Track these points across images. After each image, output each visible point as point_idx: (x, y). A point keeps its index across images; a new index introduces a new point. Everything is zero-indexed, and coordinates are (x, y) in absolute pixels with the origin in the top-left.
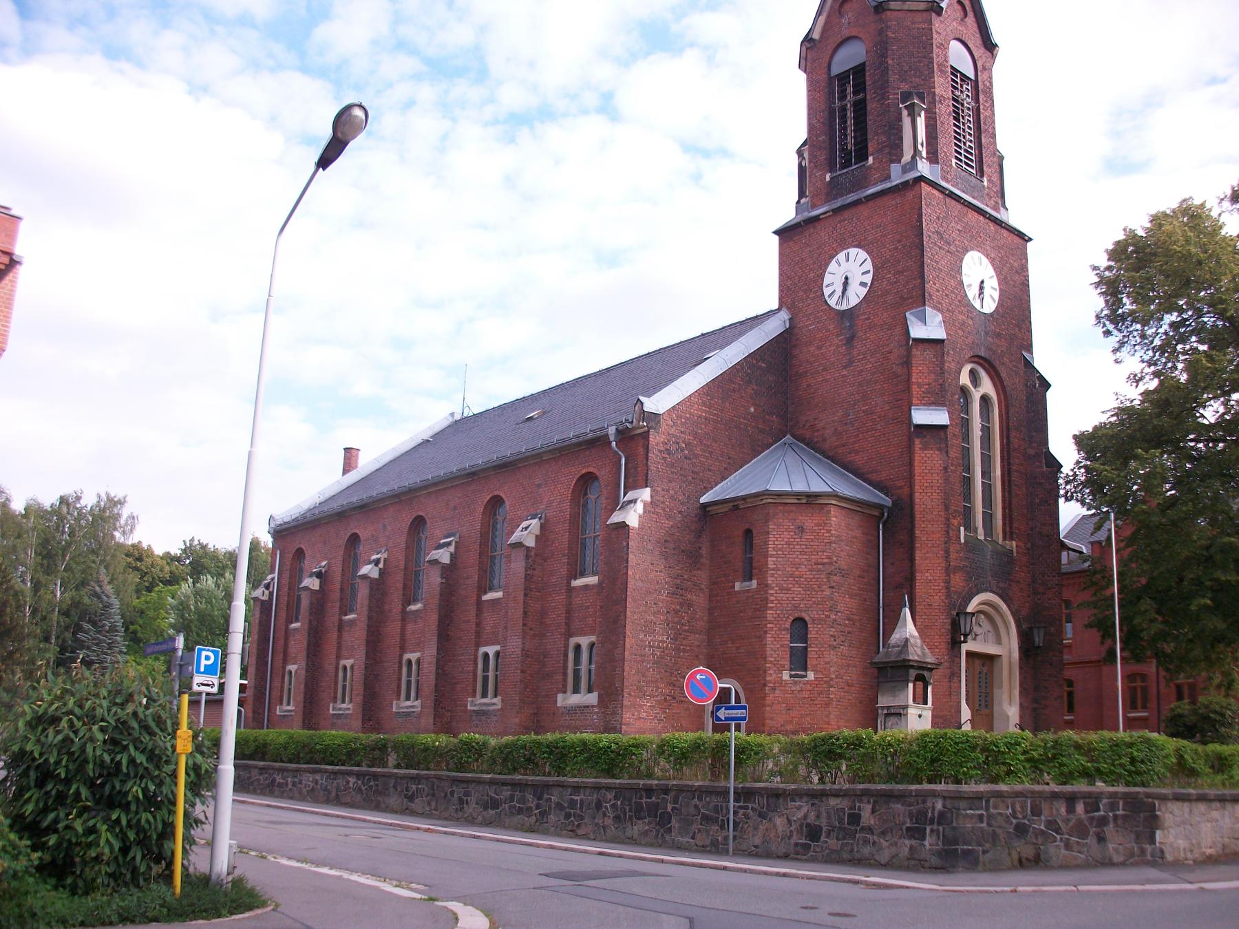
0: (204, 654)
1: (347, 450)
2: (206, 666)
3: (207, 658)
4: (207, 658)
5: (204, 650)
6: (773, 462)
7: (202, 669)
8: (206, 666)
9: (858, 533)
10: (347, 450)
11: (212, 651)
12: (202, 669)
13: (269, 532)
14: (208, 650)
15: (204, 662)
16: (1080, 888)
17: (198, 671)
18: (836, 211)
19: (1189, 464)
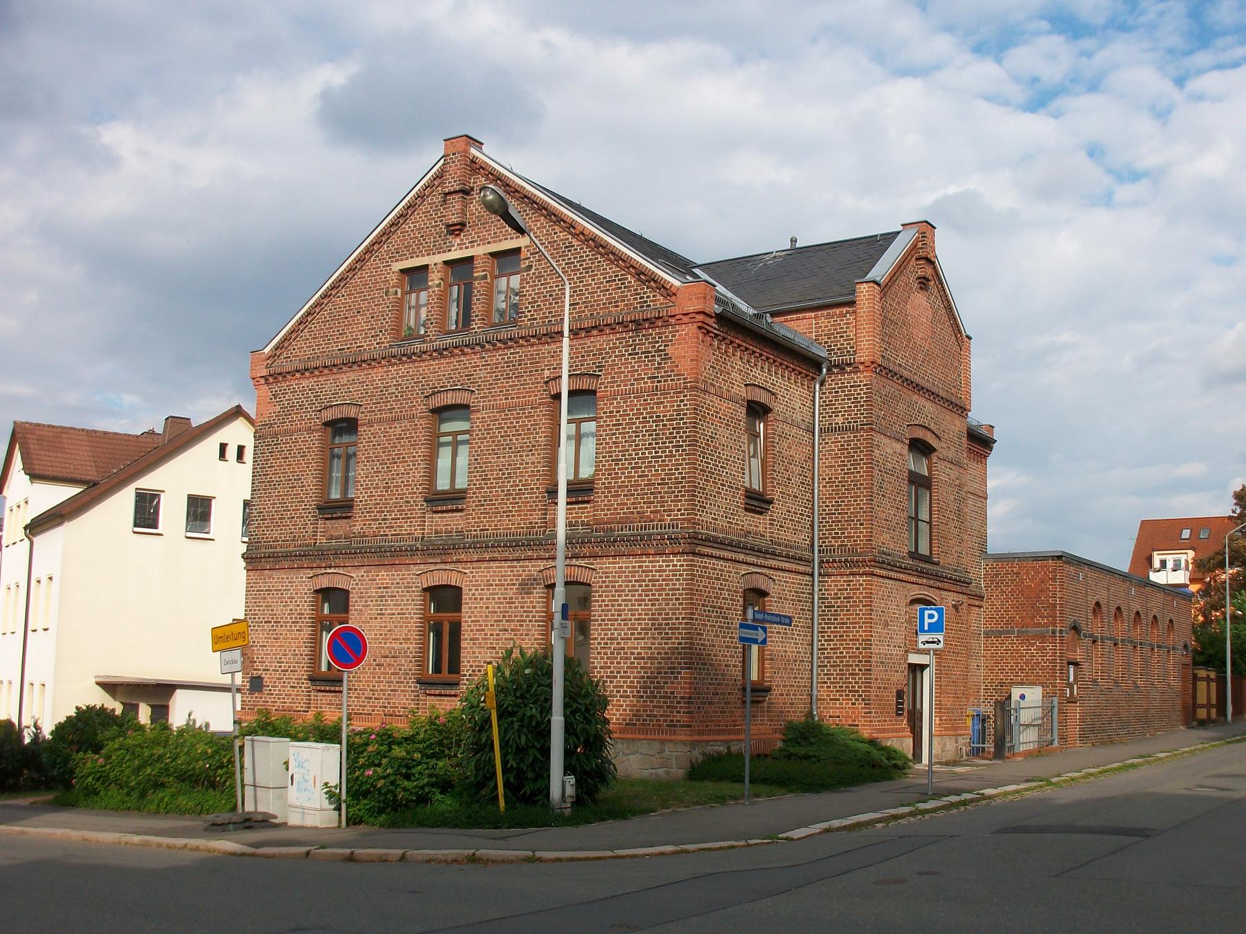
0: (927, 613)
1: (239, 446)
2: (929, 624)
3: (931, 616)
4: (931, 616)
5: (927, 609)
6: (1214, 739)
7: (926, 628)
8: (929, 624)
9: (7, 794)
10: (239, 446)
11: (935, 610)
12: (926, 628)
13: (970, 338)
14: (931, 609)
15: (927, 621)
16: (742, 843)
17: (923, 630)
18: (1100, 772)
19: (491, 200)
